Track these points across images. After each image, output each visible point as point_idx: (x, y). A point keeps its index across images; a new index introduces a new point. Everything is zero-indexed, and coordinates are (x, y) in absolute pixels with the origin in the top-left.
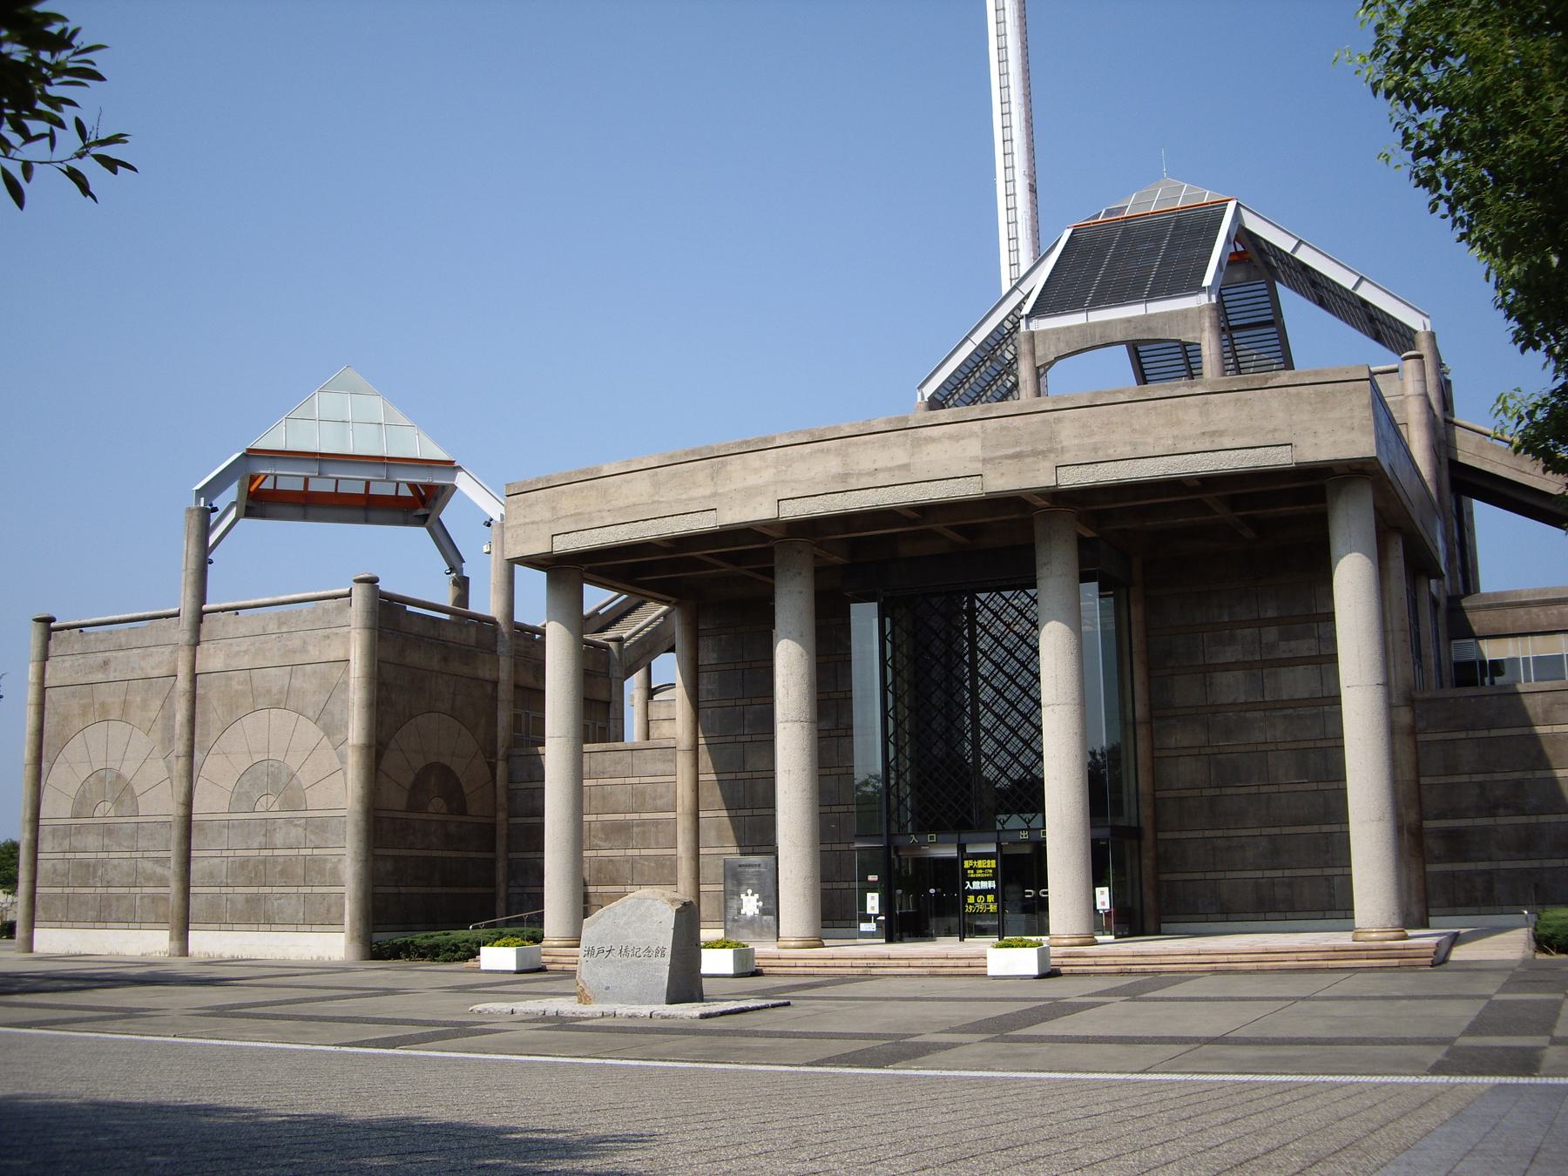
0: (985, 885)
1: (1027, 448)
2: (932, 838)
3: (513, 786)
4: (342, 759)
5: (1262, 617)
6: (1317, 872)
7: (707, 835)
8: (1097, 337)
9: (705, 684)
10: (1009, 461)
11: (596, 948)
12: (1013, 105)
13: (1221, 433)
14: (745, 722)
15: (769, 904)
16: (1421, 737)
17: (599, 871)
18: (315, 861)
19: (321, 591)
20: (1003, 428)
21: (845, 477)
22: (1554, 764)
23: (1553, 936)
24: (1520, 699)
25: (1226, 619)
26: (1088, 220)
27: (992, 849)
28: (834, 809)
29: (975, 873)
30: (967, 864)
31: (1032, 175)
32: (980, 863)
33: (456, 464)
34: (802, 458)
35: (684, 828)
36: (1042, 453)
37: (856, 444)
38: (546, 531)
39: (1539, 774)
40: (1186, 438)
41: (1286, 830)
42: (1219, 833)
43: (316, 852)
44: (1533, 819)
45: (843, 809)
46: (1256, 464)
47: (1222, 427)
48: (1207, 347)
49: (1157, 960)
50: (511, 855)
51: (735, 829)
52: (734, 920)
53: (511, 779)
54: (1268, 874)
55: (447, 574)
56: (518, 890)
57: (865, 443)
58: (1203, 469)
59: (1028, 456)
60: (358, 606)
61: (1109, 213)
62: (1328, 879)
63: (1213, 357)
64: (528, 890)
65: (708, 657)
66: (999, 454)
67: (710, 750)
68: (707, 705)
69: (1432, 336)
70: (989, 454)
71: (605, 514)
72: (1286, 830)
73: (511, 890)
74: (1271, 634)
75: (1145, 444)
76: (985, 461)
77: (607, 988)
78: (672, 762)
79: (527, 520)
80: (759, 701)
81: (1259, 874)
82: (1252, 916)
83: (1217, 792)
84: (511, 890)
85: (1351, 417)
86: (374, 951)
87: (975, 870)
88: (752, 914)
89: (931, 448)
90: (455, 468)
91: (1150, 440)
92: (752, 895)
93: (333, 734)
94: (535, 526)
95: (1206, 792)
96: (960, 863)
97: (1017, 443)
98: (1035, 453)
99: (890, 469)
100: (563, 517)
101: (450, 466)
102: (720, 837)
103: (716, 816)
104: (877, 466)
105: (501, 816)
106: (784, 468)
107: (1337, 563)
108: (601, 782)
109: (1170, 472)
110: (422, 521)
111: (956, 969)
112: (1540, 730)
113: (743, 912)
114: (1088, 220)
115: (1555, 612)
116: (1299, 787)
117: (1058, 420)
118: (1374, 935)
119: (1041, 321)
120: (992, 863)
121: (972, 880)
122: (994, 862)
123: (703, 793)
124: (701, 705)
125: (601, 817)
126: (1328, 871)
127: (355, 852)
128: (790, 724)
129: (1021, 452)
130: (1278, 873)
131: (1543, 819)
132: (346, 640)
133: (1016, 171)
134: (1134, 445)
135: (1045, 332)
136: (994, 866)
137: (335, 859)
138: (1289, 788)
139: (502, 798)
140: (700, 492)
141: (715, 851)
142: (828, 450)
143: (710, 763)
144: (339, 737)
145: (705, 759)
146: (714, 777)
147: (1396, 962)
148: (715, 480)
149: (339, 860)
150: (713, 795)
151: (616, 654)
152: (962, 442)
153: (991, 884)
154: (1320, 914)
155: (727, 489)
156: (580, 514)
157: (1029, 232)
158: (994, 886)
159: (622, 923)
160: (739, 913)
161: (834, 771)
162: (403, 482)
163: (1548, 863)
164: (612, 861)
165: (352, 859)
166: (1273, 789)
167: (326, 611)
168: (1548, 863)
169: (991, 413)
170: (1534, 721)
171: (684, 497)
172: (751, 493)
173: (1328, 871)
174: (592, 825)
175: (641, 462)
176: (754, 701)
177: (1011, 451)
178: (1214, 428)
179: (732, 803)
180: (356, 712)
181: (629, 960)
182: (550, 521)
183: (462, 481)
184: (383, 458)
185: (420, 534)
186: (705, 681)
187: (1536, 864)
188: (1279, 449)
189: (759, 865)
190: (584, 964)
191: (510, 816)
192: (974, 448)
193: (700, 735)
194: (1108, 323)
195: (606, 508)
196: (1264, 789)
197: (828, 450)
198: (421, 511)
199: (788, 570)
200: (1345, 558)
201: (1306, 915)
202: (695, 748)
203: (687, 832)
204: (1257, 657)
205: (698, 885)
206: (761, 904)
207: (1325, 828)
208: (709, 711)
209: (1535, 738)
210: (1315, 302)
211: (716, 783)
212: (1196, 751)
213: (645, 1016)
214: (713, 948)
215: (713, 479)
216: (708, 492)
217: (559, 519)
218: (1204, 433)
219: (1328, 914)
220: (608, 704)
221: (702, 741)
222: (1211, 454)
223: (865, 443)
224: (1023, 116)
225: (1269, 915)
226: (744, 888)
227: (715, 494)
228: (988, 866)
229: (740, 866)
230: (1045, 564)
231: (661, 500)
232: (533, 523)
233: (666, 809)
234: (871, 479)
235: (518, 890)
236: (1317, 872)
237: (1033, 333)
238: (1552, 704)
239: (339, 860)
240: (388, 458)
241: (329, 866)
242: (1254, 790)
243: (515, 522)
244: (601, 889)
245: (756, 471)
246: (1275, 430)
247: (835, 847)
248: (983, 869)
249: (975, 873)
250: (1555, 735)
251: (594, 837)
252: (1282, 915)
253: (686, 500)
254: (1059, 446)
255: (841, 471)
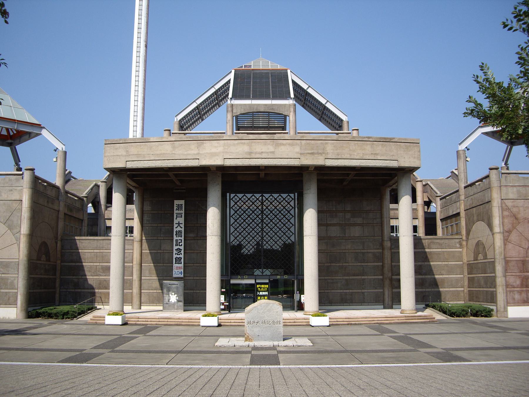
0: (264, 293)
1: (316, 151)
2: (246, 277)
3: (63, 251)
4: (18, 240)
5: (346, 210)
6: (360, 291)
7: (145, 272)
8: (255, 109)
9: (145, 218)
10: (309, 155)
11: (251, 321)
12: (143, 17)
13: (376, 154)
14: (162, 232)
15: (181, 298)
16: (393, 251)
17: (100, 284)
18: (3, 279)
19: (8, 171)
20: (308, 144)
21: (250, 153)
22: (430, 261)
23: (456, 312)
24: (422, 241)
25: (334, 209)
26: (239, 68)
27: (267, 281)
28: (195, 265)
29: (261, 289)
30: (258, 286)
31: (146, 42)
32: (263, 286)
33: (42, 126)
34: (234, 145)
35: (137, 269)
36: (321, 153)
37: (255, 142)
38: (124, 159)
39: (426, 263)
40: (367, 154)
41: (351, 278)
42: (330, 278)
43: (3, 275)
44: (424, 277)
45: (198, 265)
46: (387, 165)
47: (377, 152)
48: (292, 117)
49: (356, 320)
50: (62, 277)
51: (157, 270)
52: (167, 304)
53: (62, 247)
54: (345, 291)
55: (15, 166)
56: (65, 290)
57: (258, 142)
58: (371, 165)
59: (316, 154)
60: (28, 180)
61: (245, 66)
62: (363, 293)
63: (294, 121)
64: (69, 290)
65: (147, 208)
66: (306, 152)
67: (147, 242)
68: (146, 225)
69: (348, 122)
70: (303, 152)
71: (151, 156)
72: (351, 278)
73: (61, 290)
74: (348, 216)
75: (354, 155)
76: (301, 154)
77: (258, 336)
78: (131, 245)
79: (115, 154)
80: (167, 225)
81: (342, 291)
82: (339, 304)
83: (329, 264)
84: (61, 290)
85: (415, 154)
86: (30, 315)
87: (261, 288)
88: (174, 302)
89: (282, 147)
90: (41, 127)
91: (356, 154)
92: (174, 295)
93: (13, 229)
94: (118, 157)
95: (326, 265)
96: (256, 286)
97: (312, 149)
98: (318, 153)
99: (267, 153)
100: (131, 155)
101: (39, 127)
102: (150, 273)
103: (149, 265)
104: (262, 151)
105: (59, 262)
106: (227, 147)
107: (402, 198)
108: (101, 251)
109: (361, 165)
110: (10, 145)
111: (290, 323)
112: (427, 250)
113: (170, 301)
114: (239, 68)
115: (393, 212)
116: (355, 264)
117: (327, 143)
118: (408, 312)
119: (235, 101)
120: (267, 286)
121: (259, 292)
122: (267, 286)
123: (144, 257)
124: (144, 225)
125: (101, 264)
126: (363, 291)
127: (24, 276)
128: (214, 237)
129: (314, 152)
130: (348, 291)
131: (427, 277)
132: (21, 192)
133: (141, 39)
134: (351, 155)
135: (237, 105)
136: (267, 287)
137: (13, 279)
138: (353, 264)
139: (59, 255)
140: (193, 152)
141: (148, 278)
142: (244, 143)
143: (147, 246)
144: (15, 230)
145: (145, 245)
146: (148, 251)
147: (428, 320)
148: (199, 148)
149: (15, 279)
150: (148, 258)
151: (86, 202)
152: (293, 147)
153: (266, 293)
154: (360, 304)
155: (204, 152)
156: (139, 154)
157: (144, 61)
158: (267, 294)
159: (261, 313)
160: (169, 301)
161: (195, 251)
162: (4, 127)
163: (427, 290)
164: (105, 280)
165: (22, 279)
166: (347, 264)
167: (10, 180)
168: (427, 290)
169: (304, 138)
170: (425, 247)
171: (186, 153)
172: (213, 155)
173: (363, 291)
174: (98, 267)
175: (168, 139)
176: (165, 225)
177: (310, 152)
178: (375, 152)
179: (156, 260)
180: (25, 221)
181: (266, 325)
182: (125, 156)
183: (44, 132)
184: (15, 120)
185: (8, 149)
186: (146, 217)
187: (424, 290)
188: (394, 161)
189: (177, 284)
190: (247, 327)
191: (61, 262)
192: (297, 149)
193: (143, 236)
194: (259, 105)
195: (152, 153)
196: (344, 264)
197: (244, 143)
198: (10, 141)
199: (215, 182)
200: (405, 197)
201: (356, 304)
202: (141, 241)
203: (138, 271)
204: (344, 223)
205: (141, 290)
206: (177, 298)
207: (363, 277)
208: (147, 227)
209: (425, 252)
210: (301, 105)
211: (435, 274)
212: (323, 251)
213: (291, 346)
214: (209, 316)
215: (198, 148)
216: (196, 152)
217: (129, 155)
218: (372, 154)
219: (363, 304)
220: (82, 220)
221: (144, 238)
222: (374, 160)
223: (258, 142)
224: (146, 21)
225: (344, 304)
226: (170, 292)
227: (198, 154)
228: (266, 287)
229: (170, 284)
230: (308, 189)
231: (175, 153)
232: (117, 155)
233: (128, 262)
234: (260, 155)
235: (65, 290)
236: (360, 291)
237: (233, 104)
238: (430, 243)
239: (15, 279)
240: (17, 120)
241: (9, 281)
242: (341, 264)
243: (109, 154)
244: (100, 291)
245: (216, 147)
246: (393, 155)
247: (195, 278)
248: (264, 288)
249: (261, 289)
250: (431, 252)
251: (98, 271)
252: (348, 304)
253: (186, 154)
254: (326, 152)
255: (249, 151)
